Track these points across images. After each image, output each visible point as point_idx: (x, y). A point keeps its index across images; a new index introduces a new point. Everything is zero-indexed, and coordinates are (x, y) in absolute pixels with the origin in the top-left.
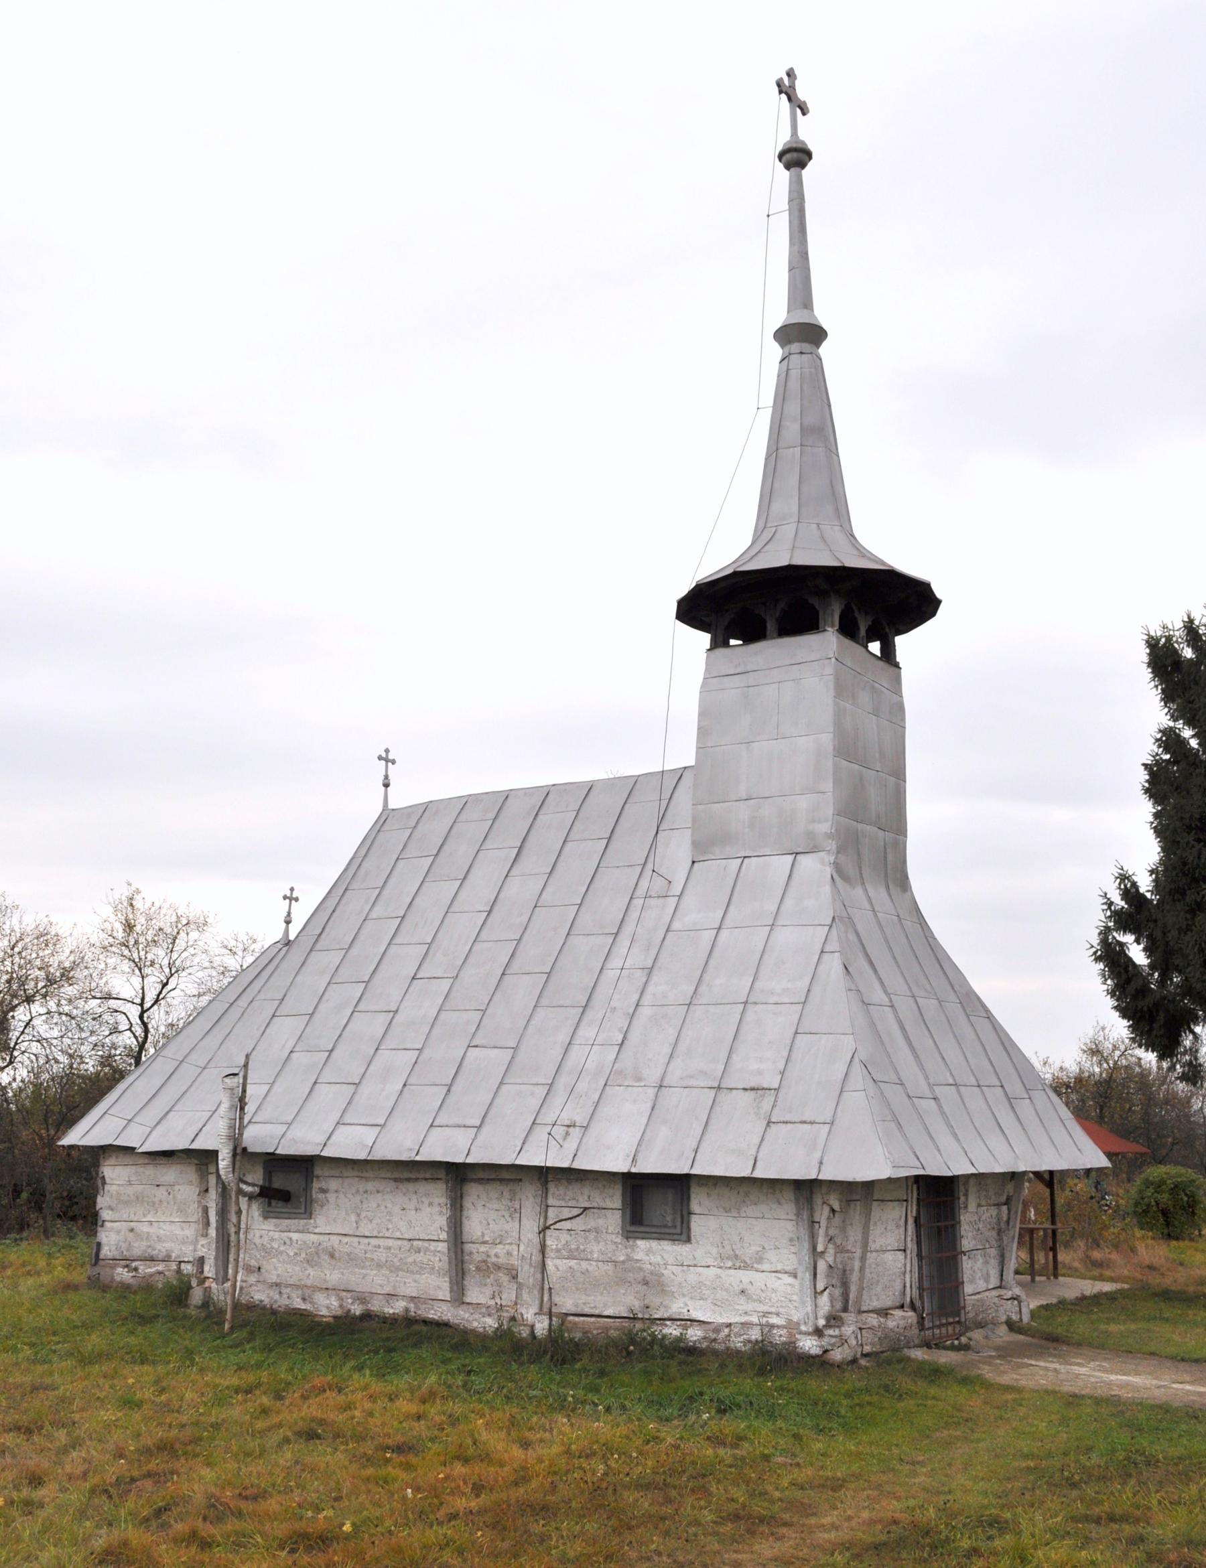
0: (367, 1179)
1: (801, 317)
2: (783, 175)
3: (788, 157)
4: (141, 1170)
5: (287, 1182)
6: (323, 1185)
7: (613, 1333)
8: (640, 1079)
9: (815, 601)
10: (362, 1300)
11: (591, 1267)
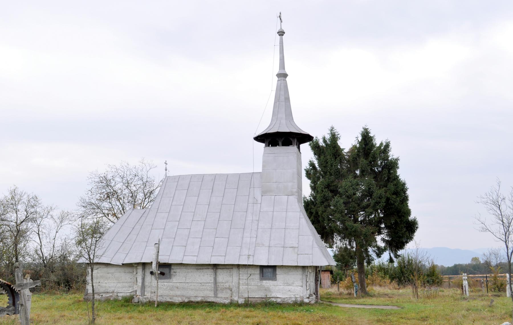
2: (278, 37)
5: (165, 269)
6: (175, 271)
7: (258, 301)
8: (263, 245)
9: (291, 139)
10: (189, 298)
11: (252, 287)
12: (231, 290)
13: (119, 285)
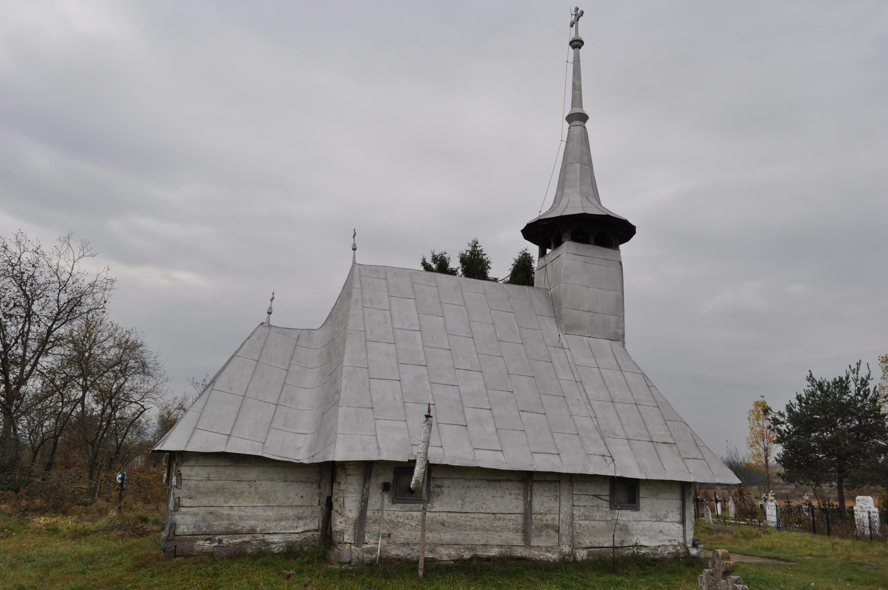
0: (469, 480)
1: (577, 110)
3: (575, 43)
4: (221, 470)
6: (439, 483)
10: (472, 548)
12: (558, 531)
13: (271, 513)
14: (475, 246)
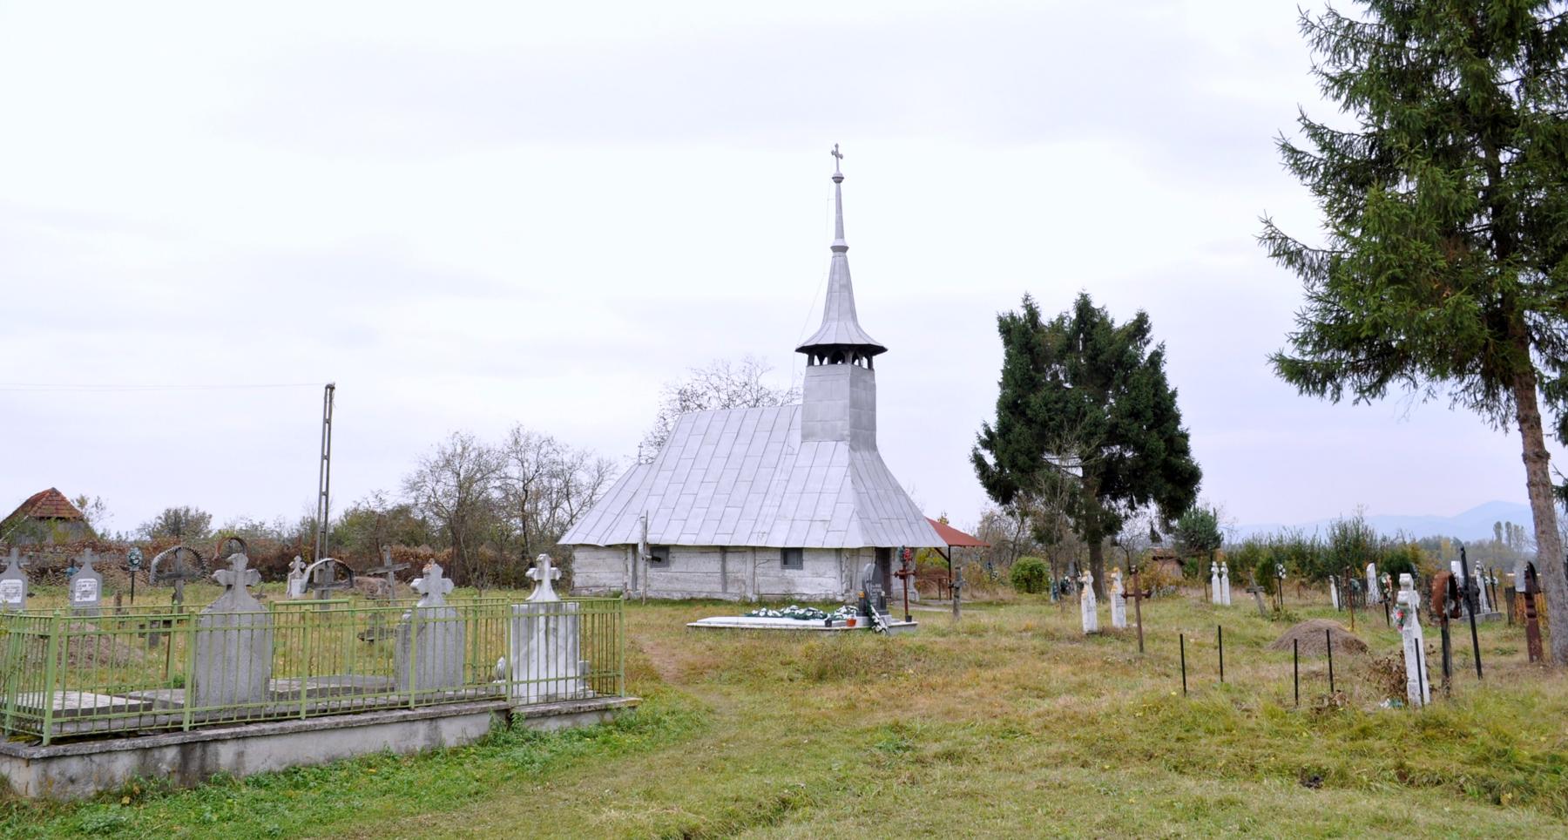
1: (839, 243)
5: (660, 554)
14: (1084, 297)
